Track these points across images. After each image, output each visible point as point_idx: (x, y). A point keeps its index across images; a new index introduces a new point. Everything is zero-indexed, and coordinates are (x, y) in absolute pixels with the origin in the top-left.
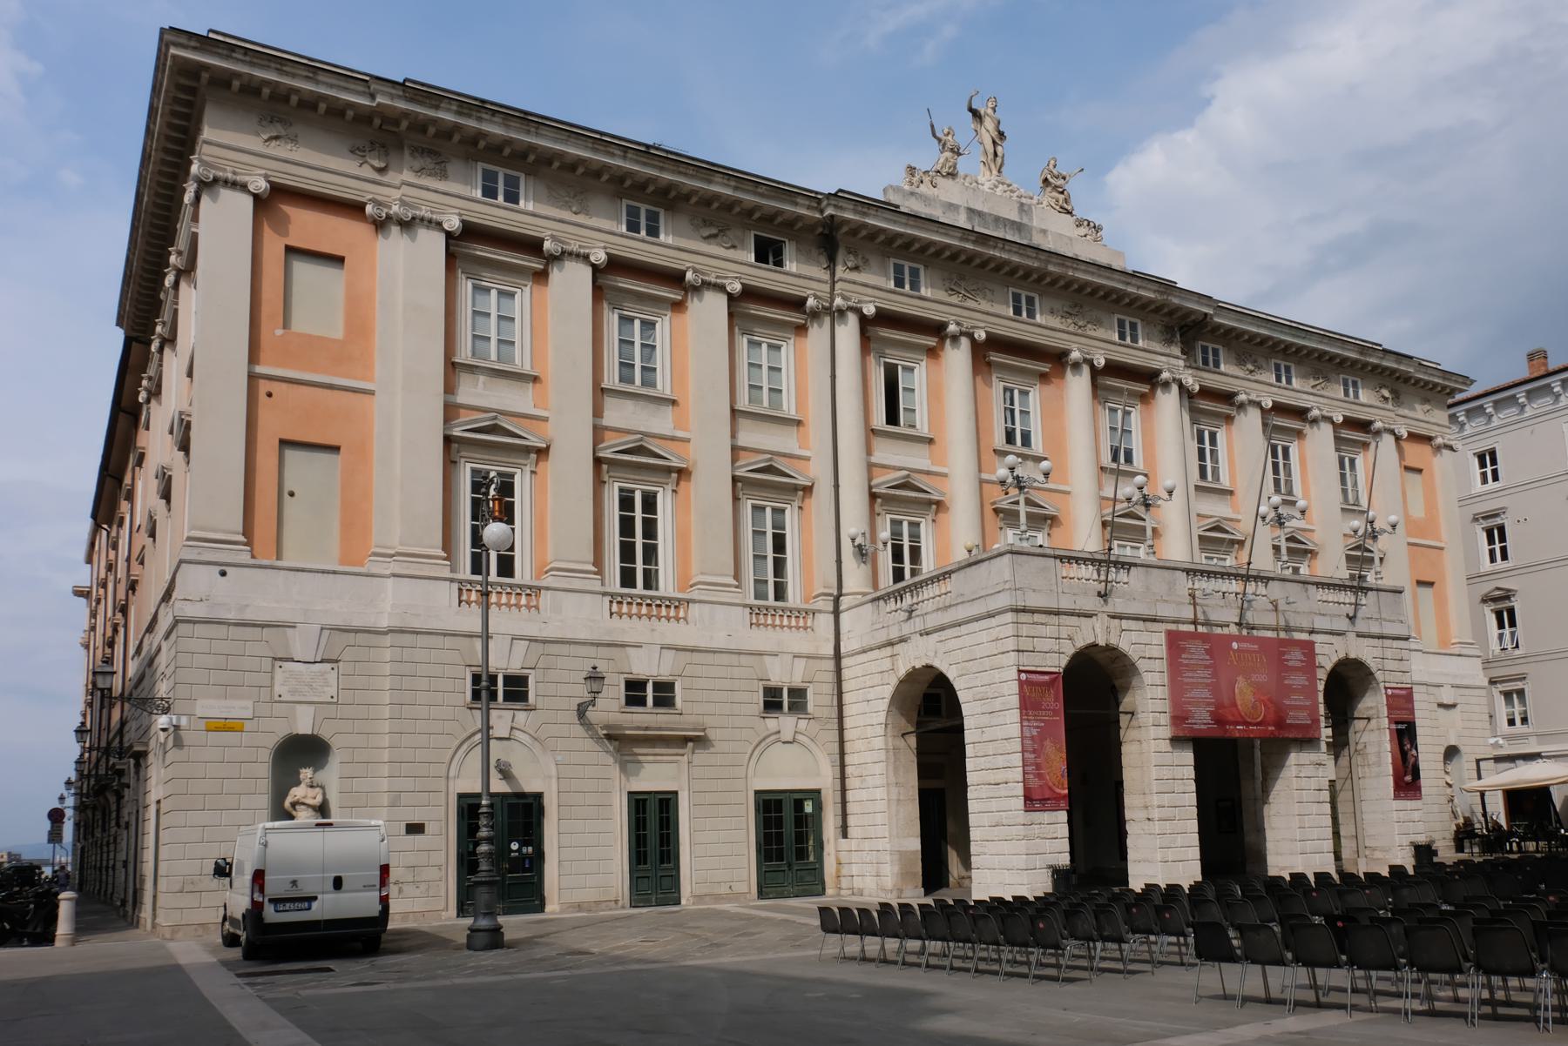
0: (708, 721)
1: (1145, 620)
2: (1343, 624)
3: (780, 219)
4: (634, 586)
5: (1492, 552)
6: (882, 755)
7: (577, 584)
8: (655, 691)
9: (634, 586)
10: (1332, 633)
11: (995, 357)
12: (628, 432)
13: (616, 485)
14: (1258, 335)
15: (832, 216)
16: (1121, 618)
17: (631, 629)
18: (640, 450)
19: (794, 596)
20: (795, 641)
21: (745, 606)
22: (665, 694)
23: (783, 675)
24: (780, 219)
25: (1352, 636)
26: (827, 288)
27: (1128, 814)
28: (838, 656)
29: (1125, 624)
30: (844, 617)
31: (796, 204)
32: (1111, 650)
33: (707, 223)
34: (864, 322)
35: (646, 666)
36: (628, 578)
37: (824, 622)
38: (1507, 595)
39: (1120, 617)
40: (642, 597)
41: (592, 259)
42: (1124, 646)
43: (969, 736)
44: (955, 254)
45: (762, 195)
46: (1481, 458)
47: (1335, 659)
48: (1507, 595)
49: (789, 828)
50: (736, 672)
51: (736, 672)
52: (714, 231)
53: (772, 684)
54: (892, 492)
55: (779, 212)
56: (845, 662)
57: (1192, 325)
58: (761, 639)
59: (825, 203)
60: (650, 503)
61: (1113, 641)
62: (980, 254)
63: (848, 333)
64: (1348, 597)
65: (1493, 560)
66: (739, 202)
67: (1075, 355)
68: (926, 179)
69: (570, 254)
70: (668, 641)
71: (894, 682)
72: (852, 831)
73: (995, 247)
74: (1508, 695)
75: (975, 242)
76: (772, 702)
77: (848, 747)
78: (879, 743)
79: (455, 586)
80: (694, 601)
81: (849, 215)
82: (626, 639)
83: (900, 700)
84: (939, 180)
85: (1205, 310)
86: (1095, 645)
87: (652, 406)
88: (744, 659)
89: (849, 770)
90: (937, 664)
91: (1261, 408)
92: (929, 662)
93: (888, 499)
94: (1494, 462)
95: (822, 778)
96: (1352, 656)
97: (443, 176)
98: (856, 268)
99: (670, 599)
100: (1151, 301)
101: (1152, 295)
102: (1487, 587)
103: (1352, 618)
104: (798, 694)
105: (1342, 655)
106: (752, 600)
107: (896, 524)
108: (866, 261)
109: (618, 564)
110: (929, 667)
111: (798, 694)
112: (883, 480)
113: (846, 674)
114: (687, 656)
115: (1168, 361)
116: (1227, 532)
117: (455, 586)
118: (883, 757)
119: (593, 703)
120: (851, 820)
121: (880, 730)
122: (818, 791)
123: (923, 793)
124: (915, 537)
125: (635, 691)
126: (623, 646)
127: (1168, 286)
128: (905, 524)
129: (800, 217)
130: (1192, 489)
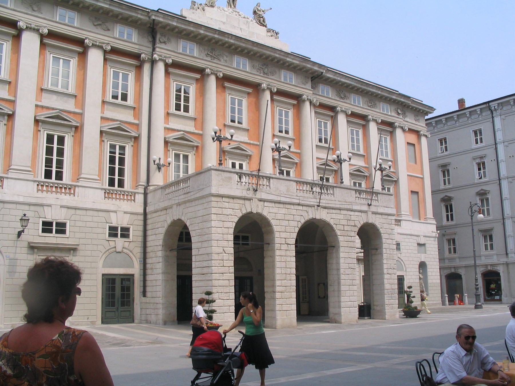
0: (82, 241)
1: (275, 203)
2: (250, 194)
3: (130, 19)
4: (50, 178)
5: (444, 181)
6: (161, 260)
7: (22, 176)
8: (117, 234)
9: (51, 178)
10: (361, 211)
11: (227, 84)
12: (53, 109)
13: (45, 132)
14: (346, 83)
15: (154, 20)
16: (264, 201)
17: (50, 197)
18: (358, 171)
19: (128, 186)
20: (125, 206)
21: (102, 189)
22: (61, 228)
23: (120, 221)
24: (168, 28)
25: (370, 213)
26: (151, 50)
27: (266, 289)
28: (145, 214)
29: (266, 204)
30: (150, 197)
31: (138, 13)
32: (259, 215)
33: (97, 19)
34: (167, 66)
35: (54, 215)
36: (111, 183)
37: (140, 198)
38: (450, 199)
39: (264, 201)
40: (117, 191)
41: (40, 31)
42: (265, 213)
43: (194, 252)
44: (210, 40)
45: (122, 9)
46: (441, 140)
47: (362, 223)
48: (450, 199)
49: (118, 292)
50: (95, 219)
51: (95, 219)
52: (100, 23)
53: (113, 225)
54: (175, 141)
55: (131, 16)
56: (149, 216)
57: (316, 76)
58: (110, 204)
59: (151, 14)
60: (61, 141)
61: (260, 211)
62: (221, 40)
63: (160, 68)
64: (254, 181)
65: (445, 184)
66: (112, 11)
67: (264, 86)
68: (201, 7)
69: (31, 28)
70: (64, 204)
71: (166, 226)
72: (148, 294)
73: (231, 39)
74: (449, 241)
75: (218, 34)
76: (113, 232)
77: (148, 255)
78: (160, 254)
79: (36, 184)
80: (78, 186)
81: (161, 20)
82: (45, 202)
83: (168, 233)
84: (206, 8)
85: (322, 71)
86: (251, 213)
87: (65, 98)
88: (100, 214)
89: (148, 266)
90: (183, 219)
91: (346, 114)
92: (180, 218)
93: (173, 144)
94: (446, 142)
95: (136, 270)
96: (370, 222)
97: (39, 11)
98: (164, 42)
99: (128, 192)
100: (298, 65)
101: (298, 62)
102: (442, 195)
103: (369, 205)
104: (127, 230)
105: (365, 221)
106: (107, 187)
107: (113, 147)
108: (169, 40)
109: (108, 176)
110: (179, 220)
111: (127, 230)
112: (171, 136)
113: (149, 222)
114: (73, 211)
115: (306, 91)
116: (390, 177)
117: (36, 184)
118: (161, 260)
119: (23, 231)
120: (148, 289)
121: (160, 248)
122: (133, 275)
123: (178, 277)
124: (122, 154)
125: (47, 227)
126: (42, 205)
127: (306, 60)
128: (118, 147)
129: (140, 19)
130: (314, 147)
